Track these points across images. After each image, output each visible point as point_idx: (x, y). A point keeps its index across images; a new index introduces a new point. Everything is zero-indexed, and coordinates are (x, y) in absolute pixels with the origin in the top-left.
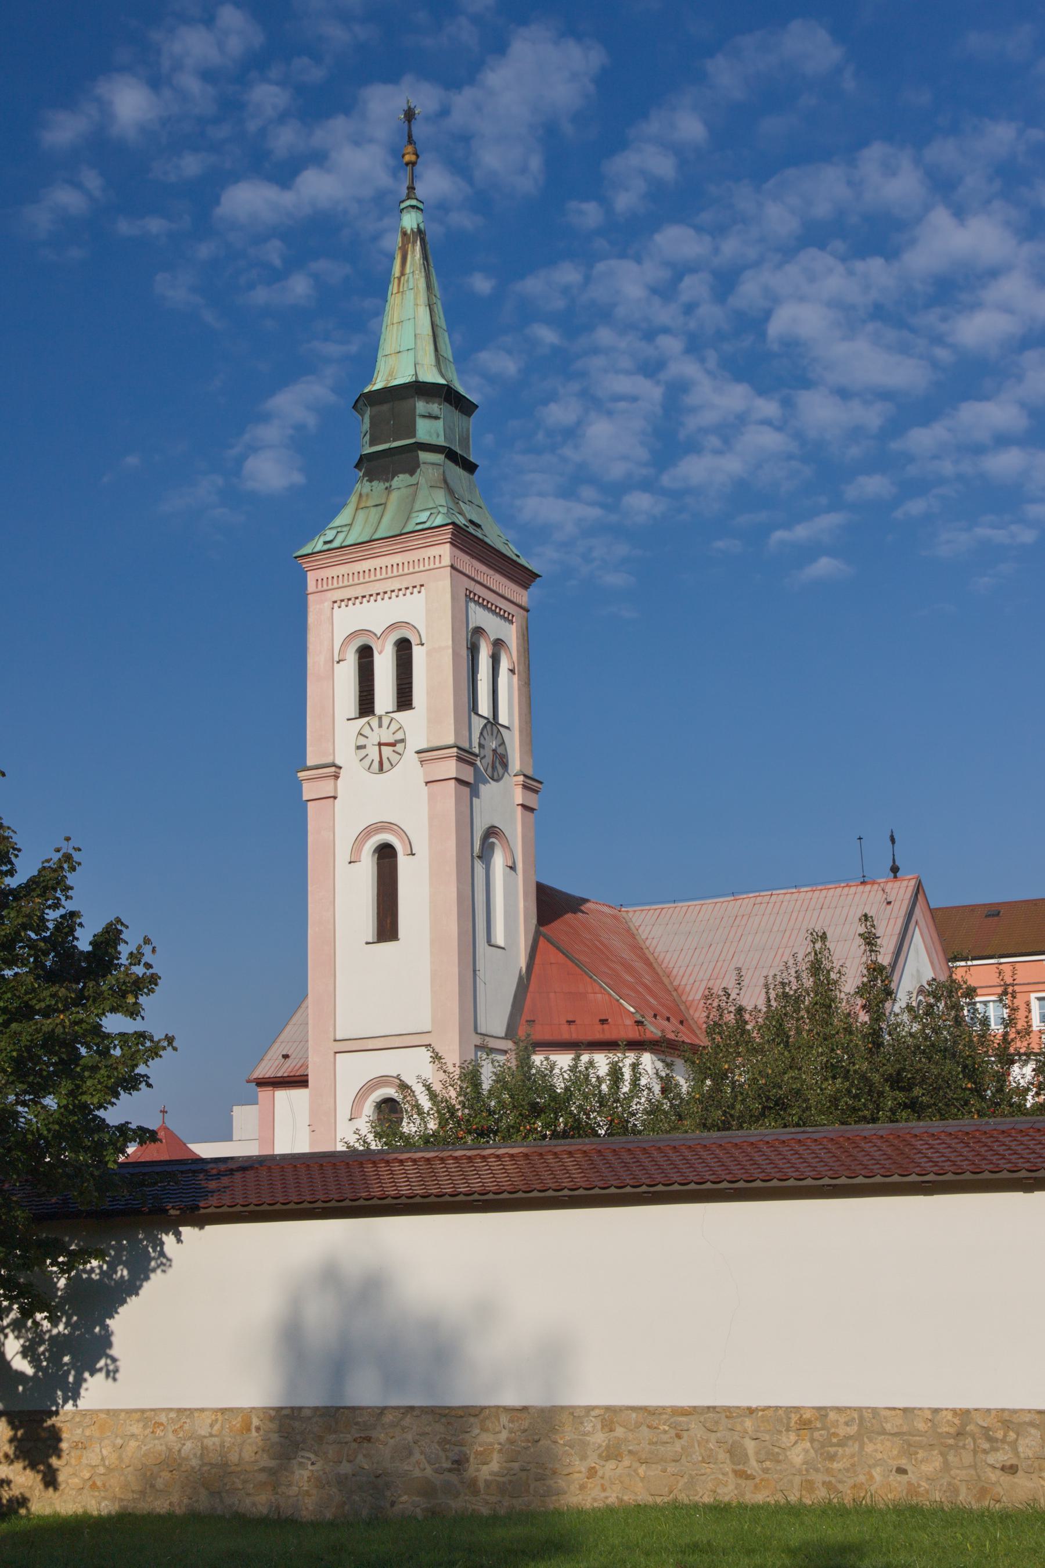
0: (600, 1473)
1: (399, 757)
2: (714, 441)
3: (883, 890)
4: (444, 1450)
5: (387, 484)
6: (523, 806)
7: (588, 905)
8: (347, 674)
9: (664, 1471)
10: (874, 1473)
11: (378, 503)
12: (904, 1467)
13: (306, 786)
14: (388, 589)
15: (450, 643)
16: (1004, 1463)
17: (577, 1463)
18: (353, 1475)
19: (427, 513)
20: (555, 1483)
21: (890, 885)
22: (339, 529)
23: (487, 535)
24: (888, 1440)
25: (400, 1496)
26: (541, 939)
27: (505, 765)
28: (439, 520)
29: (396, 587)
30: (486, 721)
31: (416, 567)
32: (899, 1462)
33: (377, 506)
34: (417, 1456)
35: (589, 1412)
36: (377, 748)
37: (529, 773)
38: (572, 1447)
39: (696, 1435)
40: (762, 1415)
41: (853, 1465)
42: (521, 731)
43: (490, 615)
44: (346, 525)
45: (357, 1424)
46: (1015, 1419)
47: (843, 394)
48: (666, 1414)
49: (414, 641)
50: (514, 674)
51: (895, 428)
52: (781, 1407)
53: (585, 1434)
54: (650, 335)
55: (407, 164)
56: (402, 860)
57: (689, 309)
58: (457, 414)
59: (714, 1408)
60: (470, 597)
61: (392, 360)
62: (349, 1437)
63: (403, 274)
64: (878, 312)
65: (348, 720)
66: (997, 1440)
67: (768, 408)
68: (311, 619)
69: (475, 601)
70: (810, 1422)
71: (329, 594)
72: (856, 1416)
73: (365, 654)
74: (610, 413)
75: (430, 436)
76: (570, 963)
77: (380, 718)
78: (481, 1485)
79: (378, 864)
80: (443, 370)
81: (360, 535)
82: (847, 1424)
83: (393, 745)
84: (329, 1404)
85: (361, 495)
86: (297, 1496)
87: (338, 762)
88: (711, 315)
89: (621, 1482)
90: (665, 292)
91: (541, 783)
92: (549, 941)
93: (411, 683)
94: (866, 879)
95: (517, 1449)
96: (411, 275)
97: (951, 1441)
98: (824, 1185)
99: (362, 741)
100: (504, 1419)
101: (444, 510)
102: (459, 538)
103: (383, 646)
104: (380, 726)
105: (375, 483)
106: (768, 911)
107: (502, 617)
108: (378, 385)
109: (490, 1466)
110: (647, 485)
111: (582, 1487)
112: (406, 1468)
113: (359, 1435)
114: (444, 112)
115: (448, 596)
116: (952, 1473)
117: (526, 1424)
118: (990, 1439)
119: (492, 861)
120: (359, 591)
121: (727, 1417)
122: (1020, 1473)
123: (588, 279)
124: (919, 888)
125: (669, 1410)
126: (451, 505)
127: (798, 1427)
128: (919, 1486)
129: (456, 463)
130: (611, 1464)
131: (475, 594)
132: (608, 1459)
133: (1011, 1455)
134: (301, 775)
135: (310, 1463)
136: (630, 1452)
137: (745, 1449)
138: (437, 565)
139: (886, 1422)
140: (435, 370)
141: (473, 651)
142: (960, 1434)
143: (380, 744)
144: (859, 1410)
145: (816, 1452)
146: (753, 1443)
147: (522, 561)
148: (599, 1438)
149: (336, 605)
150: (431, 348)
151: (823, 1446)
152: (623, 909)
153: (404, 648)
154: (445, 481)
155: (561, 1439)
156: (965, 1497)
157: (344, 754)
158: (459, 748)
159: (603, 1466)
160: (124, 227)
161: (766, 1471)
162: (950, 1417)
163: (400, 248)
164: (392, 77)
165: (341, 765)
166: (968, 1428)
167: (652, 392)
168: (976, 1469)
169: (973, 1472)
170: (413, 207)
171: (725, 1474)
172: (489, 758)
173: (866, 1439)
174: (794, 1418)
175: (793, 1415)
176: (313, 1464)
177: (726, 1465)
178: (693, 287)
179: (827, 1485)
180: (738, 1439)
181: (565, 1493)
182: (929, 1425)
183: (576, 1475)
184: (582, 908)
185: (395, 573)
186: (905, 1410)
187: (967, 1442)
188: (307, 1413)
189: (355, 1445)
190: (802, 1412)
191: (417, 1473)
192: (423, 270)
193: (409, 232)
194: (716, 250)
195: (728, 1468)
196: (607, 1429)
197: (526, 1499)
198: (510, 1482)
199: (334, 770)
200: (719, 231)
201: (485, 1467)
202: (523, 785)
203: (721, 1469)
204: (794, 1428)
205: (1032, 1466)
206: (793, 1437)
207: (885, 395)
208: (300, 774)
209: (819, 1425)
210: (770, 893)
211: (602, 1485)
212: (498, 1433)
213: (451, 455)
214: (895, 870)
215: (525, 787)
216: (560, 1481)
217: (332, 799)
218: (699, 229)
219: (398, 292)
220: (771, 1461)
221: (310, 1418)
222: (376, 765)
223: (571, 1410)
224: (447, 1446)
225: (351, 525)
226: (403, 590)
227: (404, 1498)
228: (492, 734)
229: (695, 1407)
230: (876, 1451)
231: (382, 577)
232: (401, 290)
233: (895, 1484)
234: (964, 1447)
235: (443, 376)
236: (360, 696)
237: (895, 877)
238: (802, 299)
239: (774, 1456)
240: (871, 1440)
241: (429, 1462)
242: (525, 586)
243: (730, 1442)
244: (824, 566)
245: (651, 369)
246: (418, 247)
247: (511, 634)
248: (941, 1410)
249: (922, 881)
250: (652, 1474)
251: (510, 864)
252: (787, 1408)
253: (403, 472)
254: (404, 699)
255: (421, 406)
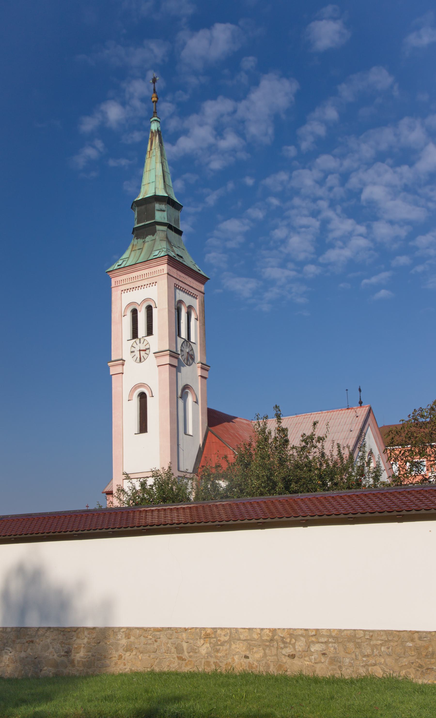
0: (123, 657)
1: (147, 355)
2: (340, 243)
3: (356, 412)
4: (62, 647)
5: (144, 240)
6: (201, 376)
7: (237, 419)
8: (127, 321)
9: (149, 657)
10: (235, 659)
11: (139, 248)
12: (248, 655)
13: (111, 369)
14: (143, 285)
15: (167, 306)
16: (289, 654)
17: (114, 653)
18: (26, 658)
19: (158, 251)
20: (105, 662)
21: (358, 409)
22: (124, 260)
23: (185, 261)
24: (241, 643)
25: (44, 667)
26: (209, 432)
27: (193, 359)
28: (162, 254)
29: (146, 284)
30: (184, 340)
31: (154, 275)
32: (246, 653)
33: (139, 249)
34: (51, 649)
35: (120, 629)
36: (139, 352)
37: (204, 362)
38: (112, 646)
39: (163, 641)
40: (190, 631)
41: (226, 654)
42: (200, 345)
43: (187, 295)
44: (127, 258)
45: (28, 635)
46: (295, 633)
47: (391, 223)
48: (151, 631)
49: (153, 306)
50: (198, 320)
51: (412, 236)
52: (198, 628)
53: (118, 640)
54: (315, 200)
55: (153, 102)
56: (149, 399)
57: (331, 189)
58: (173, 209)
59: (171, 628)
60: (176, 287)
61: (146, 187)
62: (25, 641)
63: (151, 149)
64: (406, 189)
65: (128, 340)
66: (287, 643)
67: (362, 229)
68: (113, 299)
69: (179, 289)
70: (209, 634)
71: (120, 287)
72: (229, 632)
73: (135, 312)
74: (299, 233)
75: (161, 219)
76: (220, 442)
77: (140, 339)
78: (76, 662)
79: (140, 401)
80: (167, 191)
81: (132, 261)
82: (225, 635)
83: (145, 350)
84: (18, 626)
85: (133, 245)
86: (4, 667)
87: (124, 359)
88: (339, 191)
89: (132, 662)
90: (321, 183)
91: (209, 367)
92: (212, 433)
93: (152, 324)
94: (349, 407)
95: (91, 646)
96: (154, 150)
97: (268, 644)
98: (216, 525)
99: (133, 349)
100: (86, 633)
101: (165, 250)
102: (171, 262)
103: (141, 309)
104: (140, 343)
105: (139, 240)
106: (309, 421)
107: (192, 296)
108: (140, 197)
109: (80, 654)
110: (313, 262)
111: (116, 664)
112: (47, 654)
113: (28, 640)
114: (235, 111)
115: (166, 286)
116: (267, 658)
117: (94, 636)
118: (284, 643)
119: (187, 399)
120: (131, 286)
121: (176, 632)
122: (296, 658)
123: (290, 178)
124: (370, 410)
125: (152, 629)
126: (169, 248)
127: (205, 637)
128: (253, 664)
129: (172, 230)
130: (128, 654)
131: (179, 286)
132: (126, 651)
133: (292, 650)
134: (109, 364)
135: (9, 652)
136: (136, 648)
137: (183, 647)
138: (162, 273)
139: (241, 635)
140: (163, 191)
141: (178, 311)
142: (272, 640)
143: (140, 350)
144: (230, 629)
145: (211, 648)
146: (186, 644)
147: (202, 272)
148: (124, 642)
149: (123, 292)
150: (162, 181)
151: (214, 646)
152: (253, 421)
153: (149, 309)
154: (167, 238)
155: (108, 642)
156: (273, 670)
157: (127, 356)
158: (170, 351)
159: (125, 654)
160: (112, 163)
161: (190, 657)
162: (268, 632)
163: (150, 139)
164: (214, 98)
165: (125, 360)
166: (275, 637)
167: (316, 223)
168: (277, 657)
169: (276, 657)
170: (155, 120)
171: (174, 658)
172: (186, 355)
173: (232, 642)
174: (203, 633)
175: (203, 631)
176: (10, 652)
177: (174, 654)
178: (332, 180)
179: (215, 663)
180: (180, 642)
181: (109, 666)
182: (259, 636)
183: (114, 658)
184: (233, 421)
185: (146, 278)
186: (249, 629)
187: (274, 644)
188: (9, 630)
189: (27, 644)
190: (206, 630)
191: (51, 657)
192: (159, 148)
193: (154, 131)
194: (341, 165)
195: (175, 656)
196: (127, 638)
197: (93, 669)
198: (87, 661)
199: (122, 362)
200: (342, 156)
201: (78, 655)
202: (201, 367)
203: (172, 656)
204: (203, 637)
205: (301, 655)
206: (202, 641)
207: (408, 222)
208: (109, 364)
209: (213, 636)
210: (310, 413)
211: (124, 663)
212: (83, 639)
213: (170, 227)
214: (361, 403)
215: (202, 368)
216: (107, 661)
217: (121, 374)
218: (335, 156)
219: (149, 157)
220: (193, 652)
221: (10, 632)
222: (138, 359)
223: (113, 629)
224: (63, 645)
225: (129, 258)
226: (149, 284)
227: (45, 668)
228: (187, 346)
229: (163, 628)
230: (236, 648)
231: (141, 279)
232: (150, 156)
233: (243, 663)
234: (273, 646)
235: (167, 193)
236: (133, 331)
237: (361, 406)
238: (374, 184)
239: (194, 650)
240: (234, 643)
241: (55, 652)
242: (203, 283)
243: (177, 644)
244: (383, 293)
245: (315, 214)
246: (157, 138)
247: (196, 304)
248: (264, 629)
249: (372, 407)
250: (144, 658)
251: (195, 400)
252: (200, 628)
253: (150, 235)
254: (150, 332)
255: (157, 206)
